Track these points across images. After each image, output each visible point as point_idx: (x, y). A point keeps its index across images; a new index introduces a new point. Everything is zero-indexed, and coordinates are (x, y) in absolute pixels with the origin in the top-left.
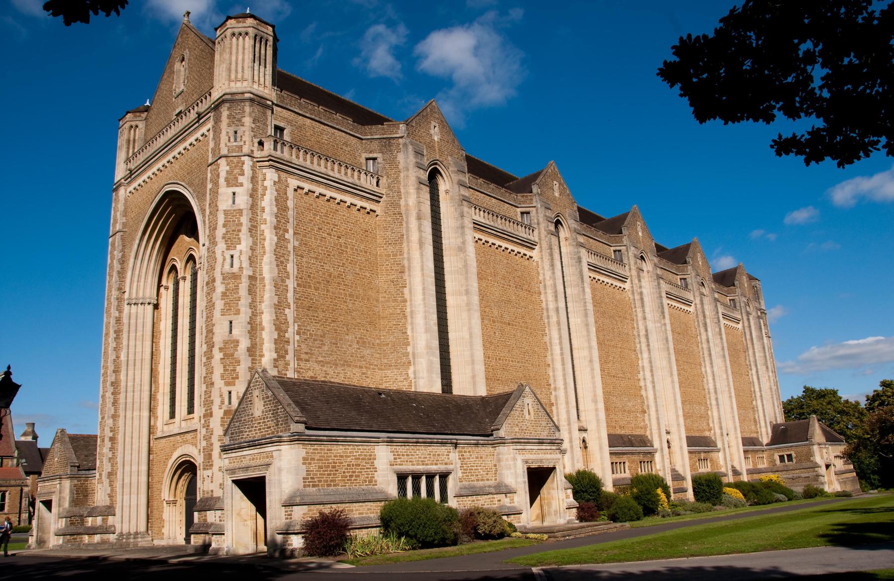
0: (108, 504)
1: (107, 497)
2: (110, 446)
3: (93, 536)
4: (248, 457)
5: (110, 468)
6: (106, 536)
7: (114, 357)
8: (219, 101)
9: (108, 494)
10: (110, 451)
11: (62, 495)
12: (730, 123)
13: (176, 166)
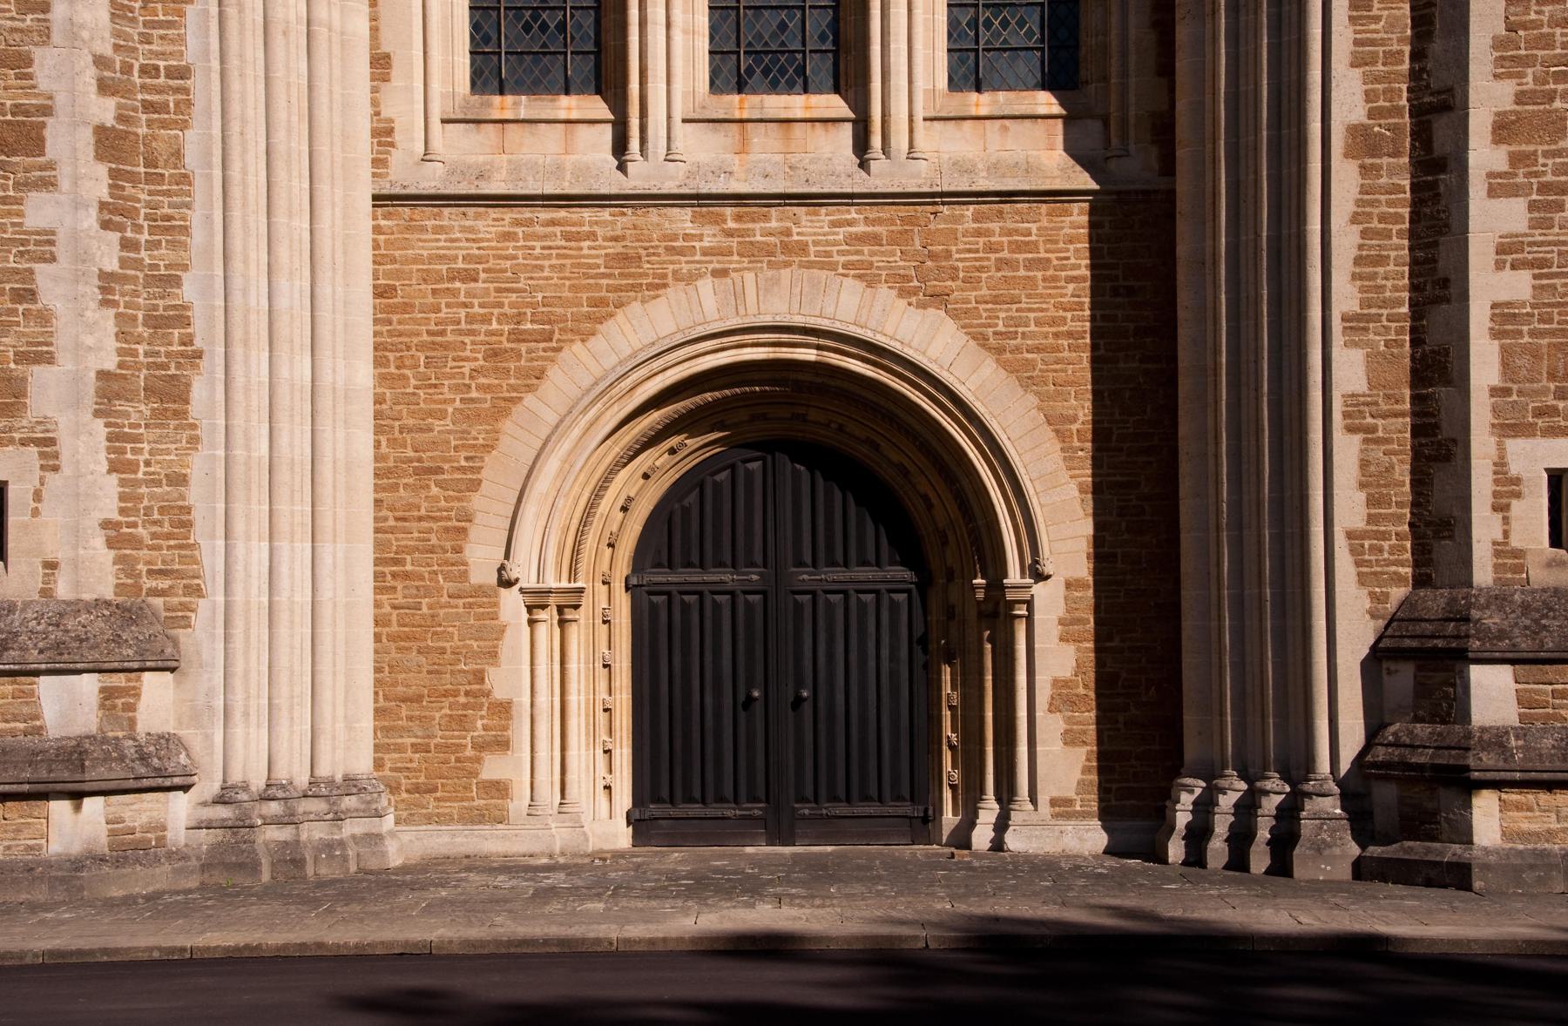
0: (108, 593)
1: (98, 541)
2: (103, 192)
3: (37, 807)
5: (112, 344)
6: (140, 810)
9: (106, 524)
10: (106, 225)
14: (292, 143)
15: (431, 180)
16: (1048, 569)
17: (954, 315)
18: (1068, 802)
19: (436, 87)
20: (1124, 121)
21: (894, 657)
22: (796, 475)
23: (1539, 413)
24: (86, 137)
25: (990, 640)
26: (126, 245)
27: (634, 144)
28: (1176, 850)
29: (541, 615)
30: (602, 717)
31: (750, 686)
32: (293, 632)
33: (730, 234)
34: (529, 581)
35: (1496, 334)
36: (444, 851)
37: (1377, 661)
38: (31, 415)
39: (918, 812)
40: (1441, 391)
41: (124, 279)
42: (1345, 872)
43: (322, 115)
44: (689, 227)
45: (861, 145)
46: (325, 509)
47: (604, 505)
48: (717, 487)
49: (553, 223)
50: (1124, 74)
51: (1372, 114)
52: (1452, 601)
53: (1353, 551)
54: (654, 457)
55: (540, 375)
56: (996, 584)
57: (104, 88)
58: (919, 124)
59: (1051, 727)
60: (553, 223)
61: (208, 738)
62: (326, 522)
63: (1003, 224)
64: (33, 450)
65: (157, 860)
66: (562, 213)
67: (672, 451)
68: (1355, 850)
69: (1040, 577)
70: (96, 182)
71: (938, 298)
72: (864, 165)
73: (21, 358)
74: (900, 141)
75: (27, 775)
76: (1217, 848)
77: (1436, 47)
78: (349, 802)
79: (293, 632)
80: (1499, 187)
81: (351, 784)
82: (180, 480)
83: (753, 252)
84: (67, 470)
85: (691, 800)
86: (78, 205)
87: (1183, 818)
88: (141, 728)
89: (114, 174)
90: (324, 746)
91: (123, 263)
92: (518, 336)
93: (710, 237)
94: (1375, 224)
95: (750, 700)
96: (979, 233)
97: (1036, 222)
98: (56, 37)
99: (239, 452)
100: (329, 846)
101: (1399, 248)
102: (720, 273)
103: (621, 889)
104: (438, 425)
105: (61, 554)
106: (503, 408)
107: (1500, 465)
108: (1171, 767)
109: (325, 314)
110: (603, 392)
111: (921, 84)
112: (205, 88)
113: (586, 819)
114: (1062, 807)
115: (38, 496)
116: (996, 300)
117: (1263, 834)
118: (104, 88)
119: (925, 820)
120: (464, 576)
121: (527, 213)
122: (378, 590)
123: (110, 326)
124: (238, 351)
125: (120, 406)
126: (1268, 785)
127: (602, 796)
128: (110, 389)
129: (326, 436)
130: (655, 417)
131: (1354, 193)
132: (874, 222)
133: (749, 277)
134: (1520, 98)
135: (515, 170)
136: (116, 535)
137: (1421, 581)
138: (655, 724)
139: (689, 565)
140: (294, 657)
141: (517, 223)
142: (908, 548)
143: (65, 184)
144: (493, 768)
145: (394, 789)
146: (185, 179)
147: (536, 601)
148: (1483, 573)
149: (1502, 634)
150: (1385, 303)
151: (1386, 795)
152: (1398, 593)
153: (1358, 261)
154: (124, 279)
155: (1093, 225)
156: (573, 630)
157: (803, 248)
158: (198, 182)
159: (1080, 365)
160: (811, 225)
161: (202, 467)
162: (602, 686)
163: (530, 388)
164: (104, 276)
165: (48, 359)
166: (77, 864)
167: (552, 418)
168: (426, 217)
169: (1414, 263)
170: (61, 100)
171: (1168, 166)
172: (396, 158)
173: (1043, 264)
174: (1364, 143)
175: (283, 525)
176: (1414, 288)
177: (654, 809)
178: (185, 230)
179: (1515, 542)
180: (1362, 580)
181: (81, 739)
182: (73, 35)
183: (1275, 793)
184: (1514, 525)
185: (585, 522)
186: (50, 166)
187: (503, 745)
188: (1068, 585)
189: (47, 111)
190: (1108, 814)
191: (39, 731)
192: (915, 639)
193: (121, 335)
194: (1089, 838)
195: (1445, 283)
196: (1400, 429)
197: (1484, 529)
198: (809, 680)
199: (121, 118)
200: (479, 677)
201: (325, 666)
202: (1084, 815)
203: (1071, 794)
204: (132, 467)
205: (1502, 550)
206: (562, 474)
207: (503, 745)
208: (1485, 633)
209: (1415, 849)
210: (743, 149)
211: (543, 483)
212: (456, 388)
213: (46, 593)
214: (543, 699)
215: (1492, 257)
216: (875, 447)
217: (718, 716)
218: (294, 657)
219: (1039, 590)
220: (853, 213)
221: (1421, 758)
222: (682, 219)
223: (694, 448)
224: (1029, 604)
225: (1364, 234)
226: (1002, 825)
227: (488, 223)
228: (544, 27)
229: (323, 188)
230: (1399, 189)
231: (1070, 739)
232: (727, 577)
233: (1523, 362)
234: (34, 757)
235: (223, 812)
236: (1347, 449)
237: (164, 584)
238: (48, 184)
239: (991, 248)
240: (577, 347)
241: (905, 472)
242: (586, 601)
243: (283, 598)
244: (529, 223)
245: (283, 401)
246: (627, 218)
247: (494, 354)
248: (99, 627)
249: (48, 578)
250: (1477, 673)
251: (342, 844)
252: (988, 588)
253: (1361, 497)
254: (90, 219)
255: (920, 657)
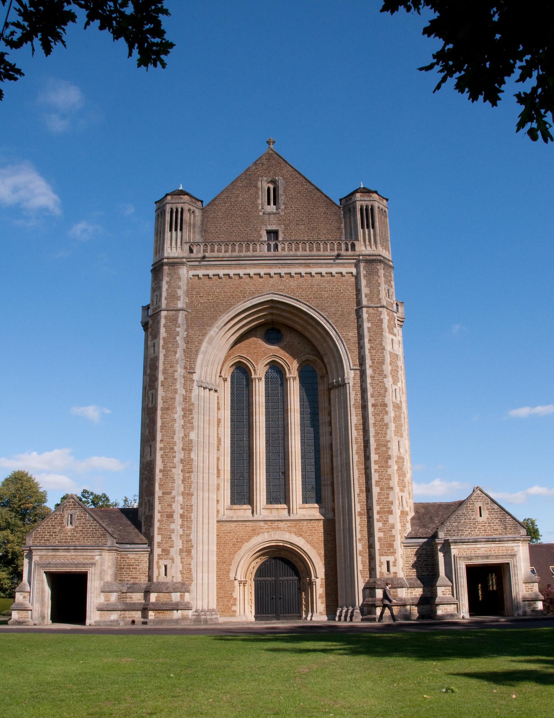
0: (180, 581)
1: (179, 573)
2: (181, 523)
3: (172, 612)
4: (484, 549)
5: (181, 545)
6: (186, 612)
7: (182, 435)
8: (374, 258)
9: (180, 571)
10: (181, 528)
11: (103, 568)
12: (13, 48)
13: (293, 283)
14: (206, 515)
15: (224, 518)
16: (318, 577)
17: (303, 538)
18: (322, 613)
19: (225, 505)
20: (328, 508)
21: (295, 591)
22: (280, 563)
23: (385, 553)
24: (179, 515)
25: (310, 588)
26: (183, 530)
27: (255, 512)
28: (337, 619)
29: (241, 585)
30: (250, 601)
31: (273, 596)
32: (205, 587)
33: (269, 526)
34: (239, 579)
35: (379, 542)
36: (227, 621)
37: (365, 589)
38: (170, 555)
39: (299, 615)
40: (372, 550)
41: (183, 535)
42: (360, 620)
43: (210, 510)
44: (263, 525)
45: (289, 512)
46: (210, 568)
47: (250, 567)
48: (268, 565)
49: (243, 524)
50: (328, 502)
51: (361, 510)
52: (374, 580)
53: (361, 573)
54: (258, 560)
55: (241, 548)
56: (310, 579)
57: (181, 508)
58: (298, 509)
59: (319, 601)
60: (243, 524)
61: (194, 602)
62: (210, 570)
63: (310, 524)
64: (171, 560)
65: (188, 620)
66: (244, 523)
67: (261, 559)
68: (361, 617)
69: (317, 578)
70: (180, 522)
71: (301, 535)
72: (289, 515)
73: (169, 547)
74: (295, 512)
75: (171, 607)
76: (343, 618)
77: (369, 501)
78: (213, 613)
79: (205, 587)
80: (378, 521)
81: (213, 610)
82: (190, 564)
83: (273, 529)
84: (175, 563)
85: (264, 614)
86: (178, 525)
87: (338, 614)
88: (185, 601)
89: (182, 520)
90: (210, 604)
91: (183, 533)
92: (237, 542)
93: (266, 526)
94: (362, 525)
95: (273, 598)
96: (307, 525)
97: (316, 524)
98: (176, 502)
99: (198, 560)
100: (211, 619)
101: (366, 529)
102: (267, 532)
103: (254, 624)
104: (225, 555)
105: (174, 575)
106: (235, 553)
107: (380, 560)
108: (337, 606)
109: (210, 540)
110: (250, 550)
111: (298, 503)
112: (194, 508)
113: (248, 616)
114: (321, 613)
115: (171, 567)
116: (310, 535)
117: (349, 615)
118: (181, 508)
119: (300, 616)
120: (229, 578)
121: (239, 523)
122: (217, 581)
123: (181, 542)
124: (198, 545)
125: (182, 554)
126: (350, 608)
127: (250, 613)
128: (181, 551)
129: (210, 557)
130: (258, 554)
131: (359, 521)
132: (292, 524)
133: (272, 532)
134: (380, 508)
135: (237, 516)
136: (182, 573)
137: (370, 577)
138: (258, 603)
139: (263, 577)
140: (205, 591)
141: (237, 525)
142: (297, 573)
143: (176, 522)
144: (234, 608)
145: (219, 611)
146: (191, 521)
147: (240, 582)
148: (378, 576)
149: (380, 585)
150: (364, 537)
151: (365, 609)
152: (367, 579)
153: (360, 531)
154: (183, 535)
155: (324, 524)
156: (246, 587)
157: (280, 528)
158: (193, 521)
159: (322, 545)
160: (281, 525)
161: (193, 562)
162: (250, 596)
163: (239, 550)
164: (181, 535)
165: (173, 547)
166: (178, 620)
167: (242, 554)
168: (224, 524)
169: (368, 531)
170: (176, 511)
171: (334, 516)
172: (219, 515)
173: (317, 530)
174: (360, 514)
175: (204, 571)
176: (368, 535)
177: (258, 615)
178: (191, 528)
179: (382, 571)
180: (362, 577)
181: (178, 602)
182: (178, 501)
183: (351, 609)
184: (382, 569)
185: (247, 570)
186: (174, 520)
187: (235, 605)
188: (321, 579)
189: (174, 512)
190: (328, 614)
191: (172, 601)
192: (225, 508)
193: (183, 543)
194: (324, 618)
195: (372, 534)
196: (367, 555)
197: (378, 569)
198: (282, 594)
199: (183, 513)
200: (231, 594)
201: (210, 592)
202: (324, 615)
203: (322, 611)
204: (183, 562)
205: (380, 573)
206: (244, 563)
207: (235, 605)
208: (378, 585)
209: (369, 616)
210: (271, 513)
211: (241, 564)
212: (228, 550)
213: (172, 581)
214: (241, 598)
215: (378, 530)
216: (292, 558)
217: (268, 600)
218: (205, 591)
219: (317, 580)
220: (288, 523)
221: (370, 603)
222: (262, 524)
223: (264, 558)
224: (315, 582)
225: (361, 527)
226: (312, 616)
227: (233, 525)
228: (241, 495)
229: (210, 521)
230: (366, 521)
231: (322, 603)
232: (269, 579)
233: (382, 545)
234: (171, 604)
235: (196, 613)
236: (359, 558)
237: (188, 580)
238: (174, 522)
239: (309, 528)
240: (246, 543)
241: (296, 562)
242: (247, 582)
243: (204, 582)
244: (239, 524)
245: (204, 553)
246: (253, 524)
247: (234, 545)
248: (179, 586)
249: (172, 579)
250: (377, 590)
251: (212, 619)
252: (309, 580)
253: (362, 565)
254: (179, 527)
255: (299, 591)
